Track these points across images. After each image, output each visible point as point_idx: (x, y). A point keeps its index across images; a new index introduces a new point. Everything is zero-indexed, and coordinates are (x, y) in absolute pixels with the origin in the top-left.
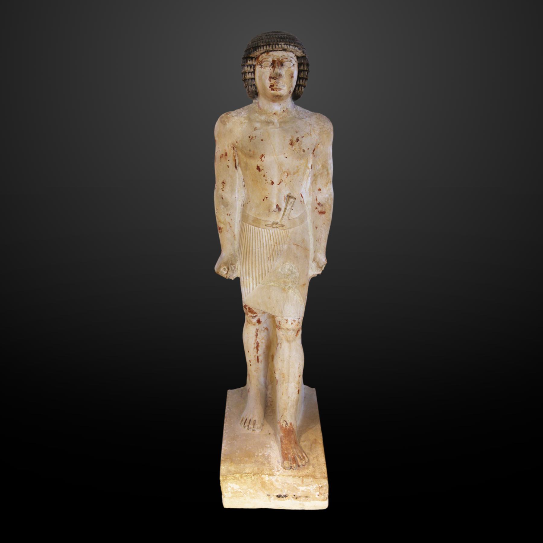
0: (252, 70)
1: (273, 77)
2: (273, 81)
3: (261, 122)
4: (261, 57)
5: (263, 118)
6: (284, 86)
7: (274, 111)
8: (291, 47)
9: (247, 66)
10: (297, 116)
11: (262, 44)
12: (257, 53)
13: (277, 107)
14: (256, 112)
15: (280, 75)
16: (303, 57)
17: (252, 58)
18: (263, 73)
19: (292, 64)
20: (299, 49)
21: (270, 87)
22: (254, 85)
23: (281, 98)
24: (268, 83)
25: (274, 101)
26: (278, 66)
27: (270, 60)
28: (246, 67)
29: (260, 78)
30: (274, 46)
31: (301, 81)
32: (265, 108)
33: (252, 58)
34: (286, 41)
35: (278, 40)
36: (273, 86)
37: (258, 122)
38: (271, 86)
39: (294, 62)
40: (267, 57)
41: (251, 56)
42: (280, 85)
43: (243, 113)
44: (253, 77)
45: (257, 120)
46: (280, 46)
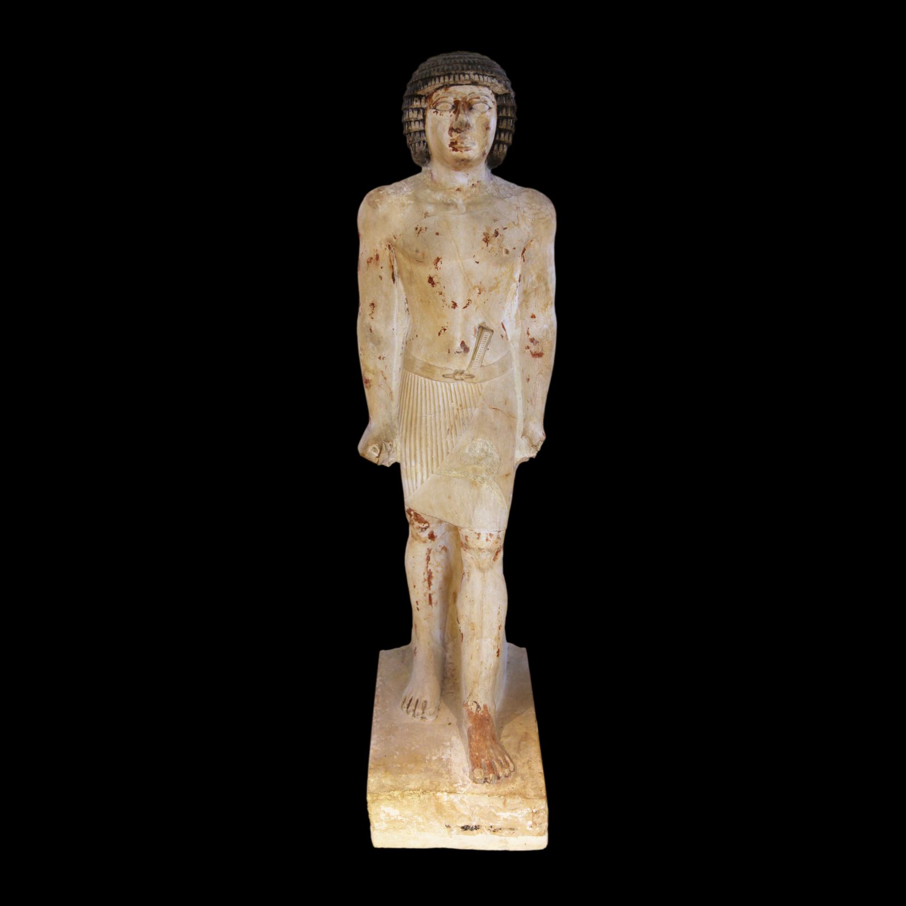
0: (421, 117)
1: (455, 128)
2: (455, 136)
3: (436, 203)
4: (435, 95)
5: (439, 196)
6: (474, 144)
7: (457, 186)
8: (485, 78)
9: (413, 110)
10: (496, 194)
11: (437, 74)
12: (428, 89)
13: (462, 179)
14: (428, 187)
15: (467, 126)
17: (420, 97)
18: (439, 122)
19: (487, 107)
20: (499, 82)
21: (450, 146)
22: (424, 142)
23: (470, 164)
24: (447, 139)
25: (457, 169)
26: (464, 110)
27: (451, 100)
29: (435, 129)
30: (457, 77)
31: (502, 135)
32: (443, 180)
33: (420, 97)
34: (478, 69)
35: (465, 66)
36: (456, 143)
37: (430, 203)
38: (453, 144)
39: (490, 104)
40: (445, 95)
41: (419, 93)
42: (468, 142)
43: (405, 189)
44: (422, 128)
45: (429, 200)
46: (467, 76)
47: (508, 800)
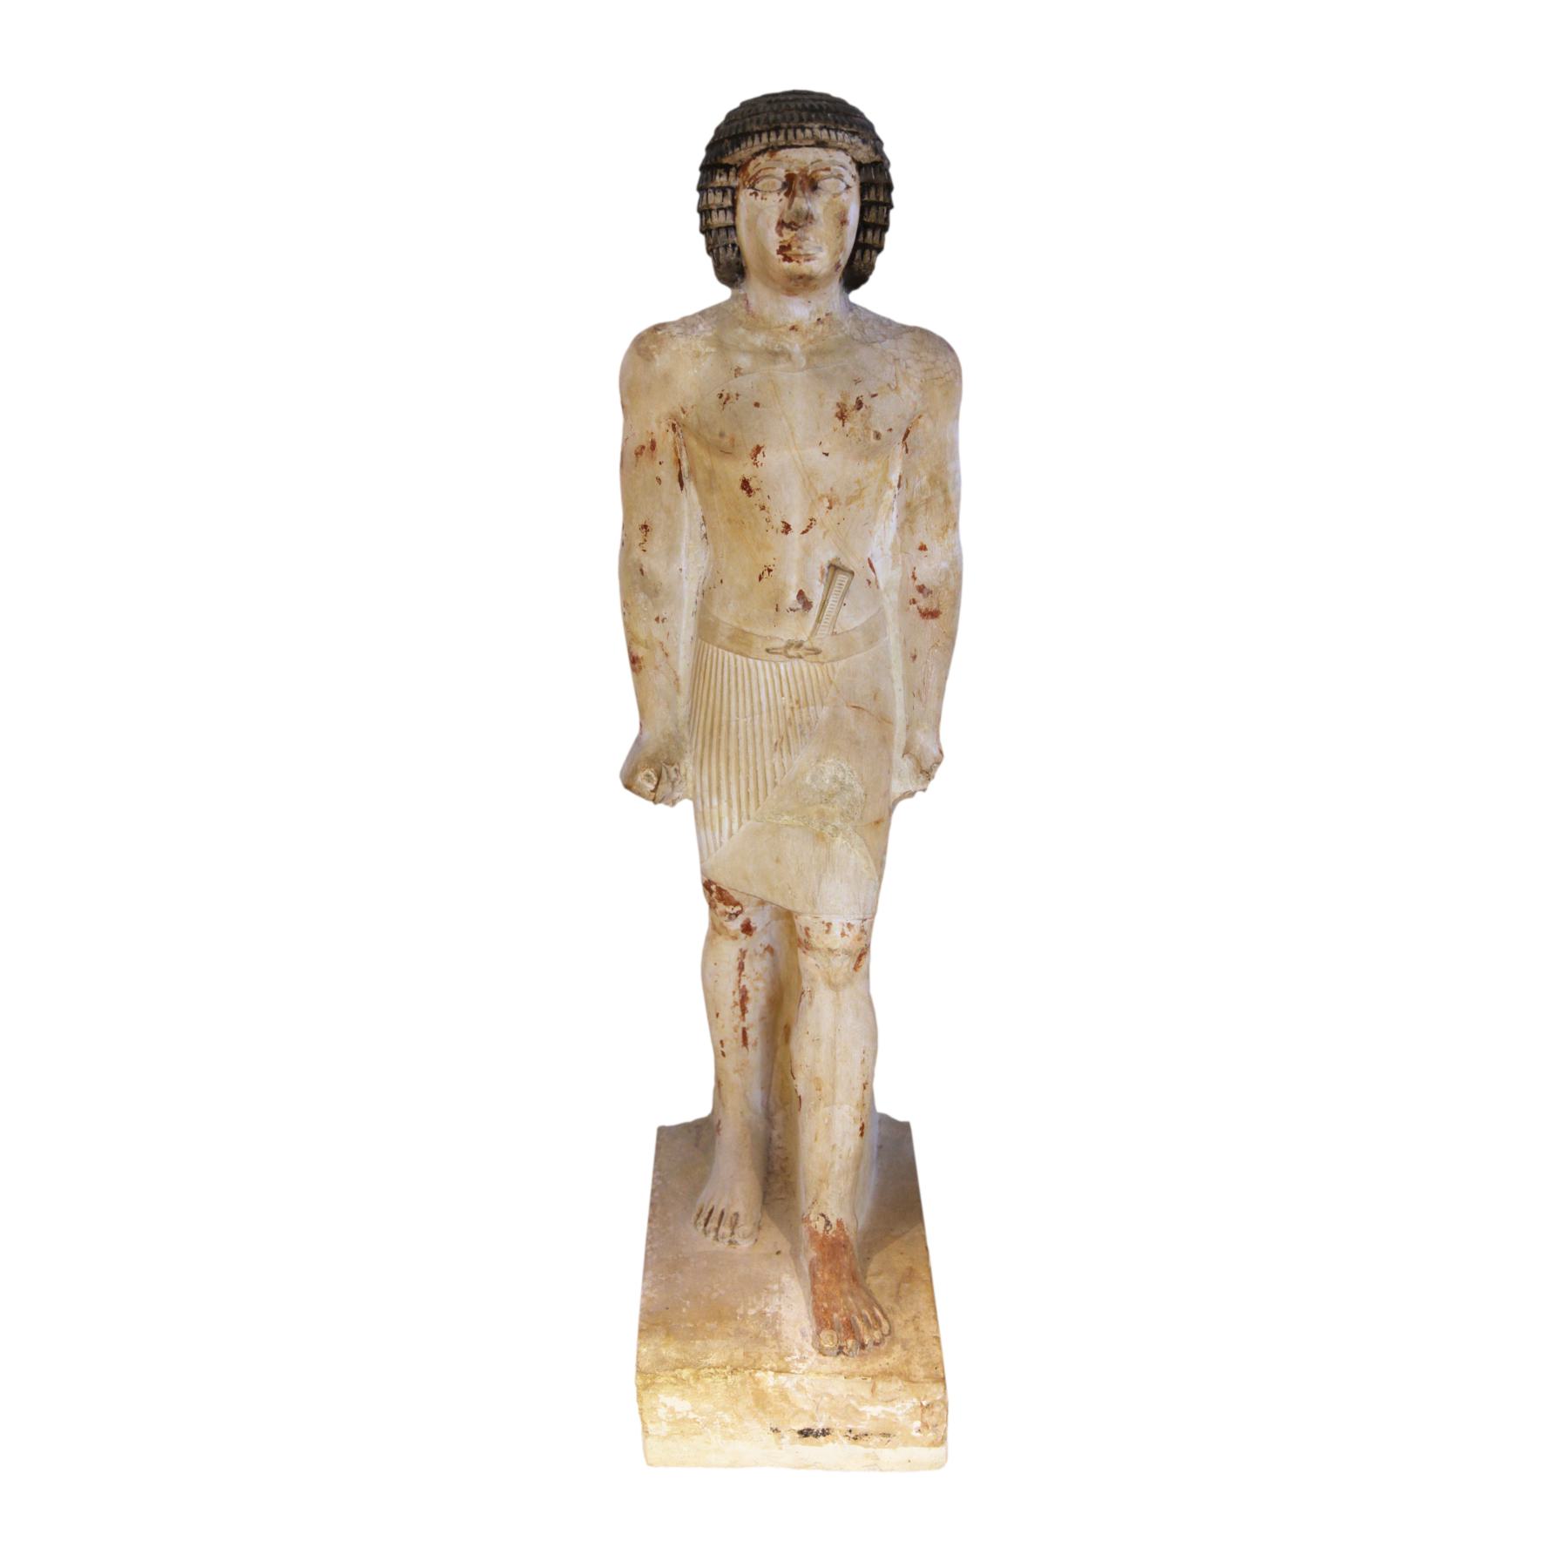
0: (728, 202)
1: (787, 221)
2: (788, 235)
3: (754, 352)
4: (752, 164)
5: (759, 340)
6: (820, 249)
7: (792, 322)
8: (840, 135)
9: (714, 190)
10: (858, 336)
11: (756, 128)
12: (741, 154)
13: (799, 310)
14: (741, 323)
15: (809, 217)
16: (875, 164)
17: (727, 168)
18: (761, 211)
19: (843, 186)
20: (864, 142)
21: (779, 252)
22: (734, 245)
23: (813, 283)
24: (773, 240)
25: (791, 292)
26: (803, 190)
27: (781, 173)
28: (711, 195)
29: (752, 224)
30: (791, 133)
31: (869, 234)
32: (767, 312)
33: (727, 168)
34: (827, 120)
35: (804, 115)
36: (789, 247)
37: (744, 352)
38: (784, 249)
39: (849, 180)
40: (771, 164)
41: (725, 161)
42: (809, 246)
43: (701, 327)
44: (730, 222)
45: (743, 345)
46: (808, 132)
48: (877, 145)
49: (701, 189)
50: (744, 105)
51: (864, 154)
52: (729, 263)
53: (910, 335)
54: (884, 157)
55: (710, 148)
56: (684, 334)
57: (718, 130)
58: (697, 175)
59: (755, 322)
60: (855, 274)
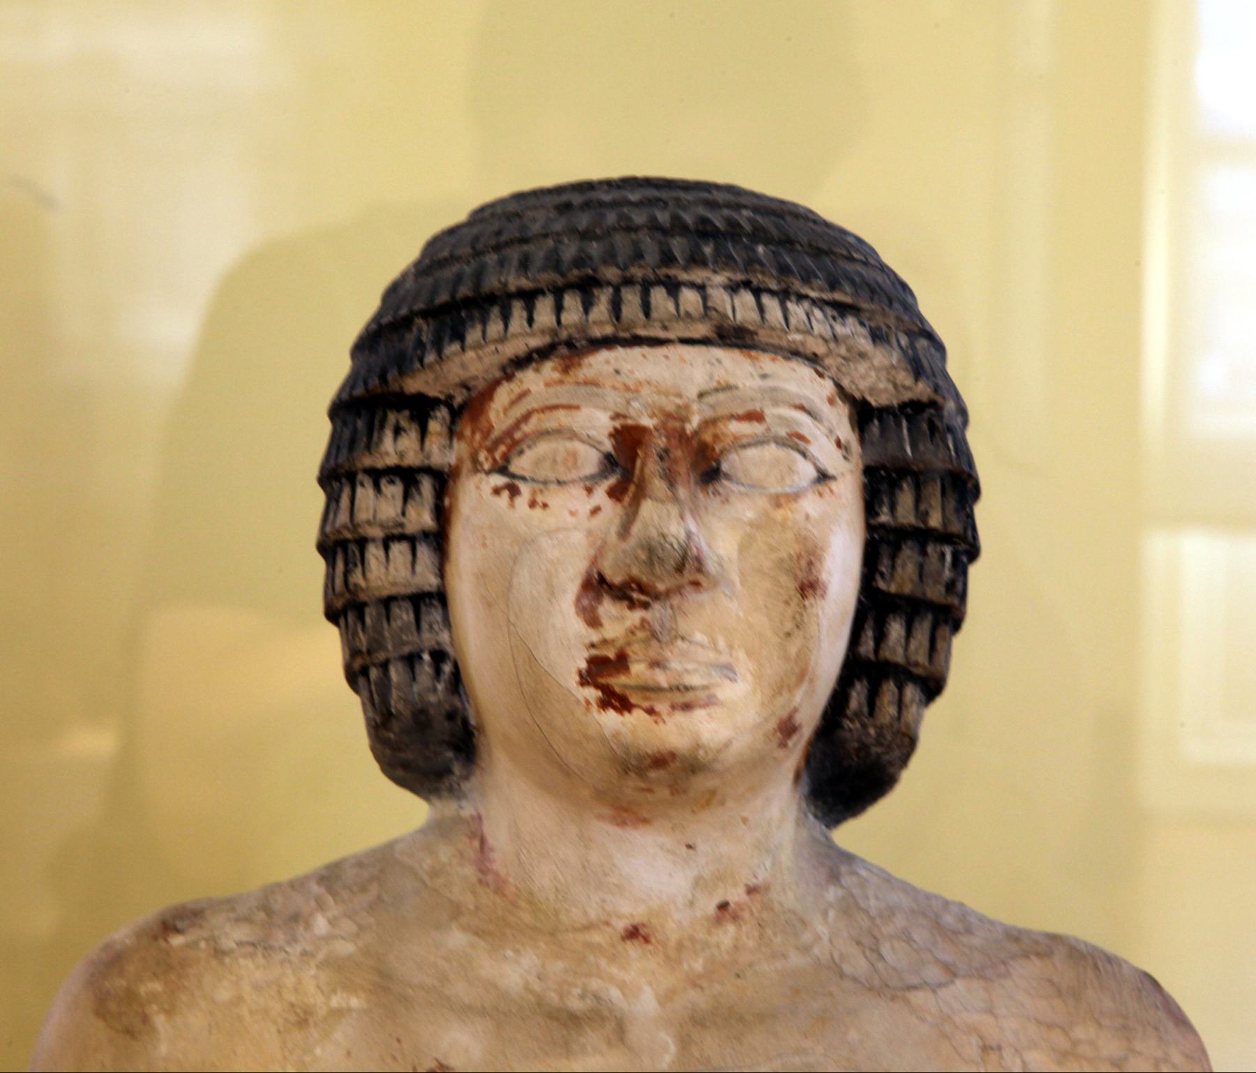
0: (421, 517)
1: (616, 578)
2: (617, 621)
3: (499, 1012)
4: (503, 395)
5: (516, 970)
6: (728, 671)
7: (628, 911)
8: (797, 311)
9: (377, 476)
10: (858, 964)
11: (515, 281)
12: (468, 361)
13: (653, 871)
14: (456, 911)
15: (689, 569)
16: (913, 410)
17: (421, 409)
18: (527, 543)
19: (807, 471)
20: (877, 337)
21: (587, 678)
22: (439, 656)
23: (702, 783)
24: (566, 638)
25: (627, 814)
26: (670, 479)
27: (597, 422)
28: (365, 494)
29: (500, 593)
30: (631, 299)
31: (896, 629)
32: (544, 878)
33: (421, 409)
34: (751, 262)
35: (678, 245)
36: (622, 662)
37: (466, 1011)
38: (603, 670)
39: (831, 459)
40: (562, 394)
41: (414, 385)
42: (687, 664)
43: (321, 924)
44: (427, 578)
45: (461, 990)
46: (689, 297)
47: (371, 518)
48: (922, 347)
49: (336, 476)
50: (481, 215)
51: (880, 375)
52: (421, 718)
53: (1035, 967)
54: (944, 386)
55: (367, 344)
56: (261, 946)
57: (393, 293)
58: (321, 431)
59: (506, 911)
60: (848, 767)
